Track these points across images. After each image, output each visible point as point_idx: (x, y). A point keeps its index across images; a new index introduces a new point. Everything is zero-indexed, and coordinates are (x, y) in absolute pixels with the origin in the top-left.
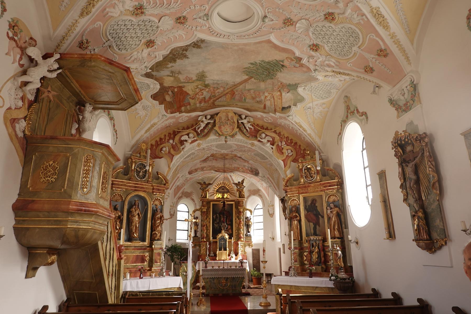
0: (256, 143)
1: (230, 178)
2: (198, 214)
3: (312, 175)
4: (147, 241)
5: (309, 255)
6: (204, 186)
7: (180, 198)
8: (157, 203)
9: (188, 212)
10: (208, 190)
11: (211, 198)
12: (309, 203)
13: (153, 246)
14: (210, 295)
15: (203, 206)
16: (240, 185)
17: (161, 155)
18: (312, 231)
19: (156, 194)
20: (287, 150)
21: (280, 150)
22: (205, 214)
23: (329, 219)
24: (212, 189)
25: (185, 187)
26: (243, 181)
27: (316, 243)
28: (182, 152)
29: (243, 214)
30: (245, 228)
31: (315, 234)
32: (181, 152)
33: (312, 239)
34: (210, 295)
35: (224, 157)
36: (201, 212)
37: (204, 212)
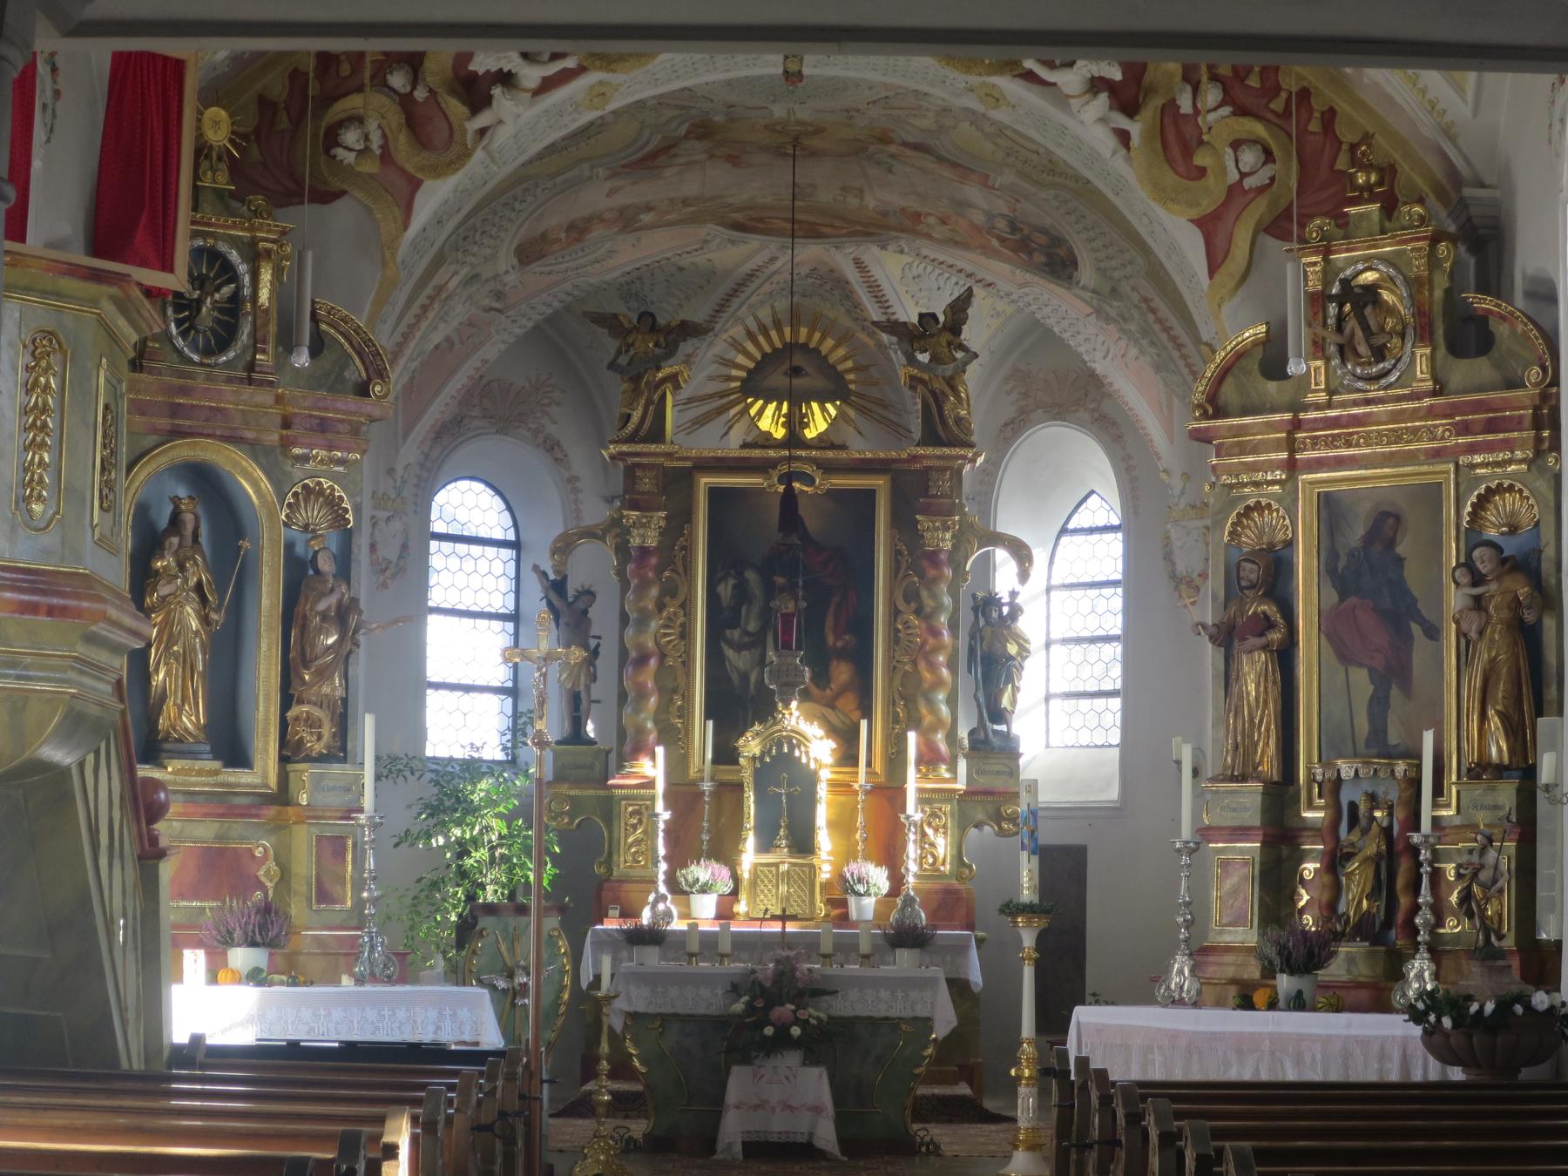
0: (1007, 85)
1: (852, 275)
3: (1379, 340)
7: (450, 433)
8: (315, 513)
9: (515, 545)
11: (707, 443)
12: (1356, 533)
15: (634, 506)
16: (939, 333)
18: (1363, 725)
19: (305, 459)
20: (1236, 145)
21: (1178, 144)
24: (701, 369)
26: (959, 308)
28: (479, 154)
30: (967, 684)
32: (466, 154)
36: (622, 550)
37: (644, 551)
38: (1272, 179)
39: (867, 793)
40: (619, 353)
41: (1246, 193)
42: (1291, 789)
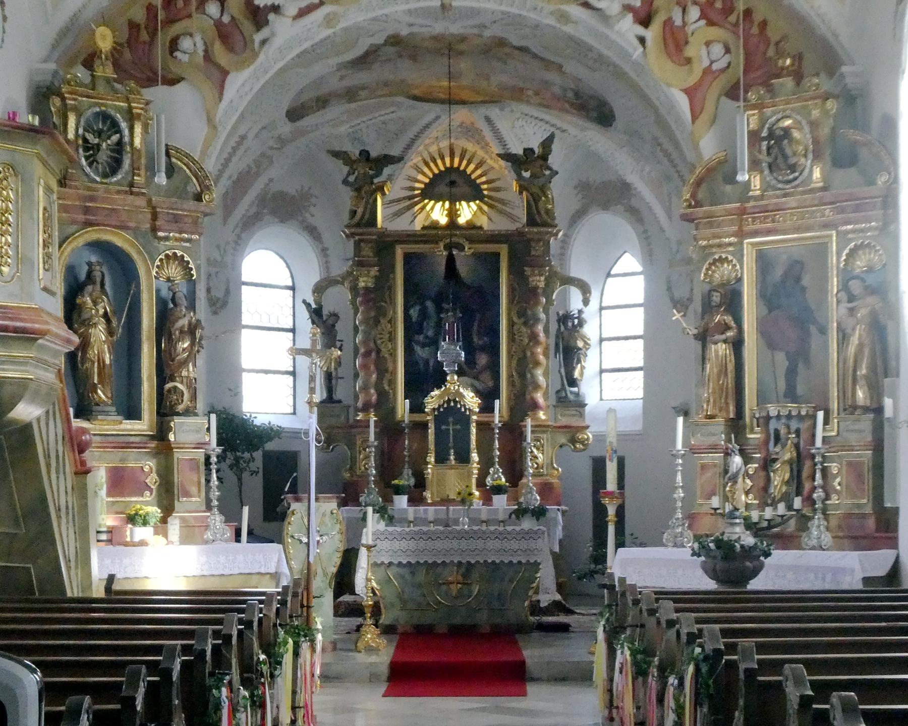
2: (339, 299)
3: (792, 161)
4: (146, 415)
5: (762, 474)
6: (362, 169)
7: (250, 223)
9: (293, 288)
10: (381, 189)
11: (401, 225)
12: (778, 273)
13: (171, 437)
14: (400, 630)
16: (531, 164)
17: (176, 70)
18: (782, 385)
19: (166, 239)
20: (708, 44)
22: (374, 300)
23: (844, 338)
25: (274, 172)
26: (547, 144)
27: (788, 427)
28: (262, 57)
29: (549, 302)
31: (791, 395)
32: (256, 55)
33: (773, 412)
34: (400, 630)
35: (449, 48)
36: (354, 289)
38: (729, 64)
39: (500, 428)
40: (349, 174)
41: (714, 72)
42: (741, 422)
